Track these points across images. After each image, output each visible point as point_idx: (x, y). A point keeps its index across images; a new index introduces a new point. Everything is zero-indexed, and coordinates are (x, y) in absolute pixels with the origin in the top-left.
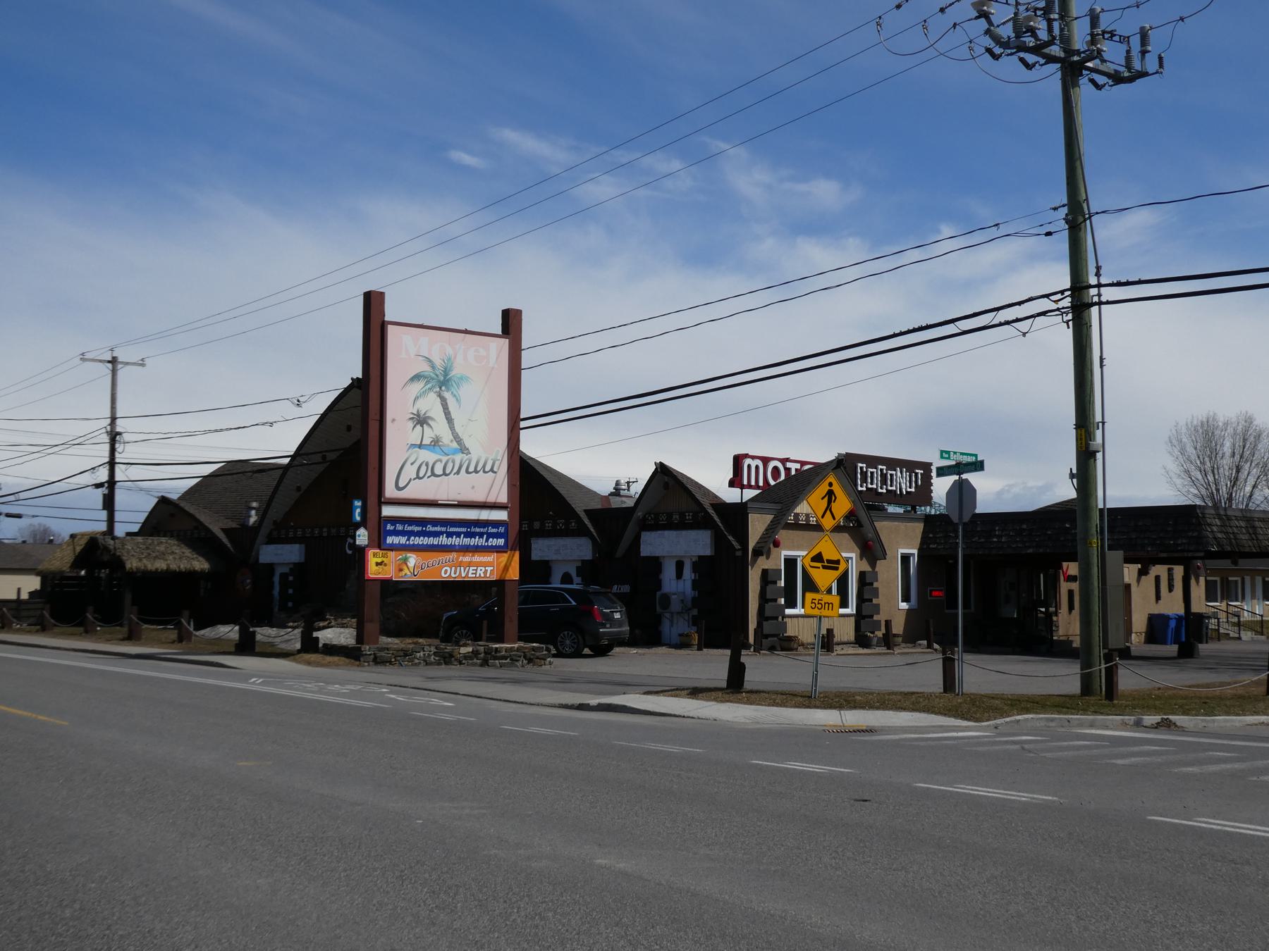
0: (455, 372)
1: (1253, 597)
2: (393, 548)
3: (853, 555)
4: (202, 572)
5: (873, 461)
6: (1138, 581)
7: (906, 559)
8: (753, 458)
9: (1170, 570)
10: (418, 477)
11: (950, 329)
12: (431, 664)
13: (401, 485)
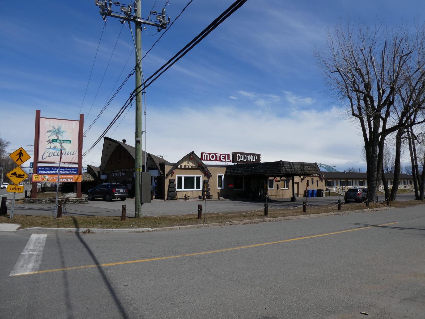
0: (62, 130)
1: (356, 185)
2: (41, 174)
3: (202, 176)
4: (92, 181)
5: (242, 154)
6: (301, 181)
7: (220, 177)
8: (206, 153)
9: (312, 179)
10: (49, 156)
11: (125, 107)
12: (47, 203)
13: (44, 158)
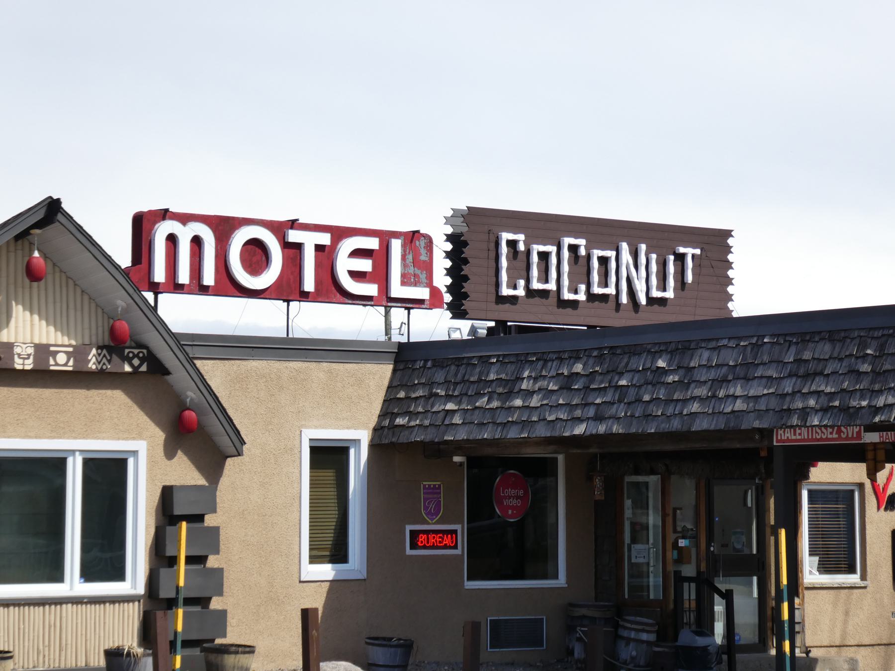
7: (329, 458)
8: (185, 219)
